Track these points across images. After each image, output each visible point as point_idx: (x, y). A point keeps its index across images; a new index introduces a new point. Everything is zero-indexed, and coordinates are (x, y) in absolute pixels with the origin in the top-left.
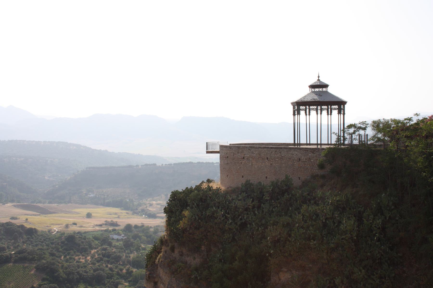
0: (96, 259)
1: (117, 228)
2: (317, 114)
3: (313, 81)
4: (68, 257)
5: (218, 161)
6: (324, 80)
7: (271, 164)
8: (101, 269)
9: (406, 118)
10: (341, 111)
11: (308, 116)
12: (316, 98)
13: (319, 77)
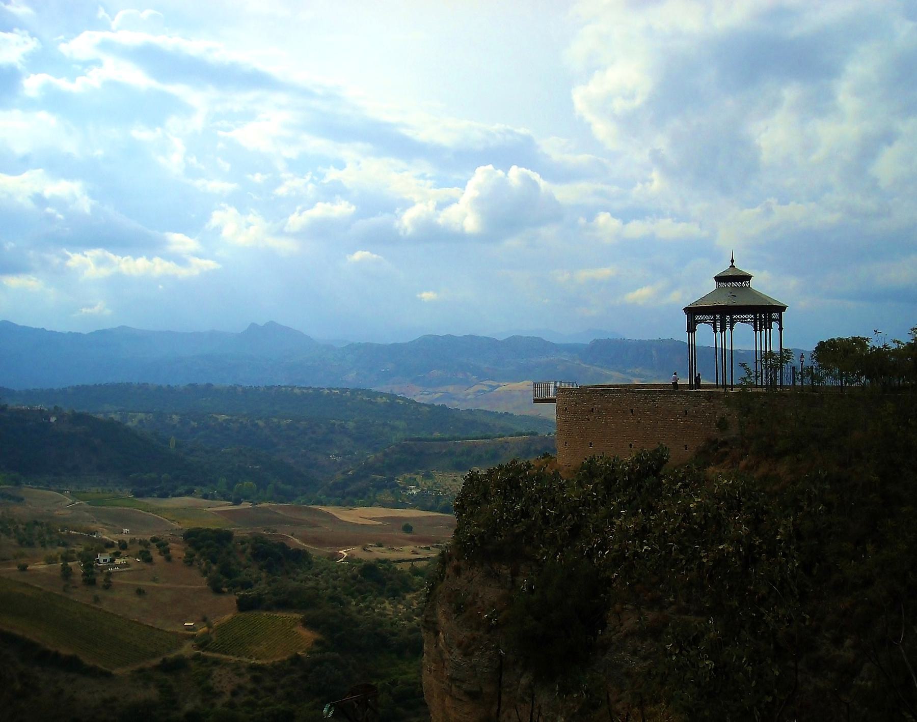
0: (413, 610)
3: (722, 268)
4: (362, 605)
5: (554, 417)
6: (743, 267)
7: (638, 422)
12: (724, 301)
13: (732, 261)
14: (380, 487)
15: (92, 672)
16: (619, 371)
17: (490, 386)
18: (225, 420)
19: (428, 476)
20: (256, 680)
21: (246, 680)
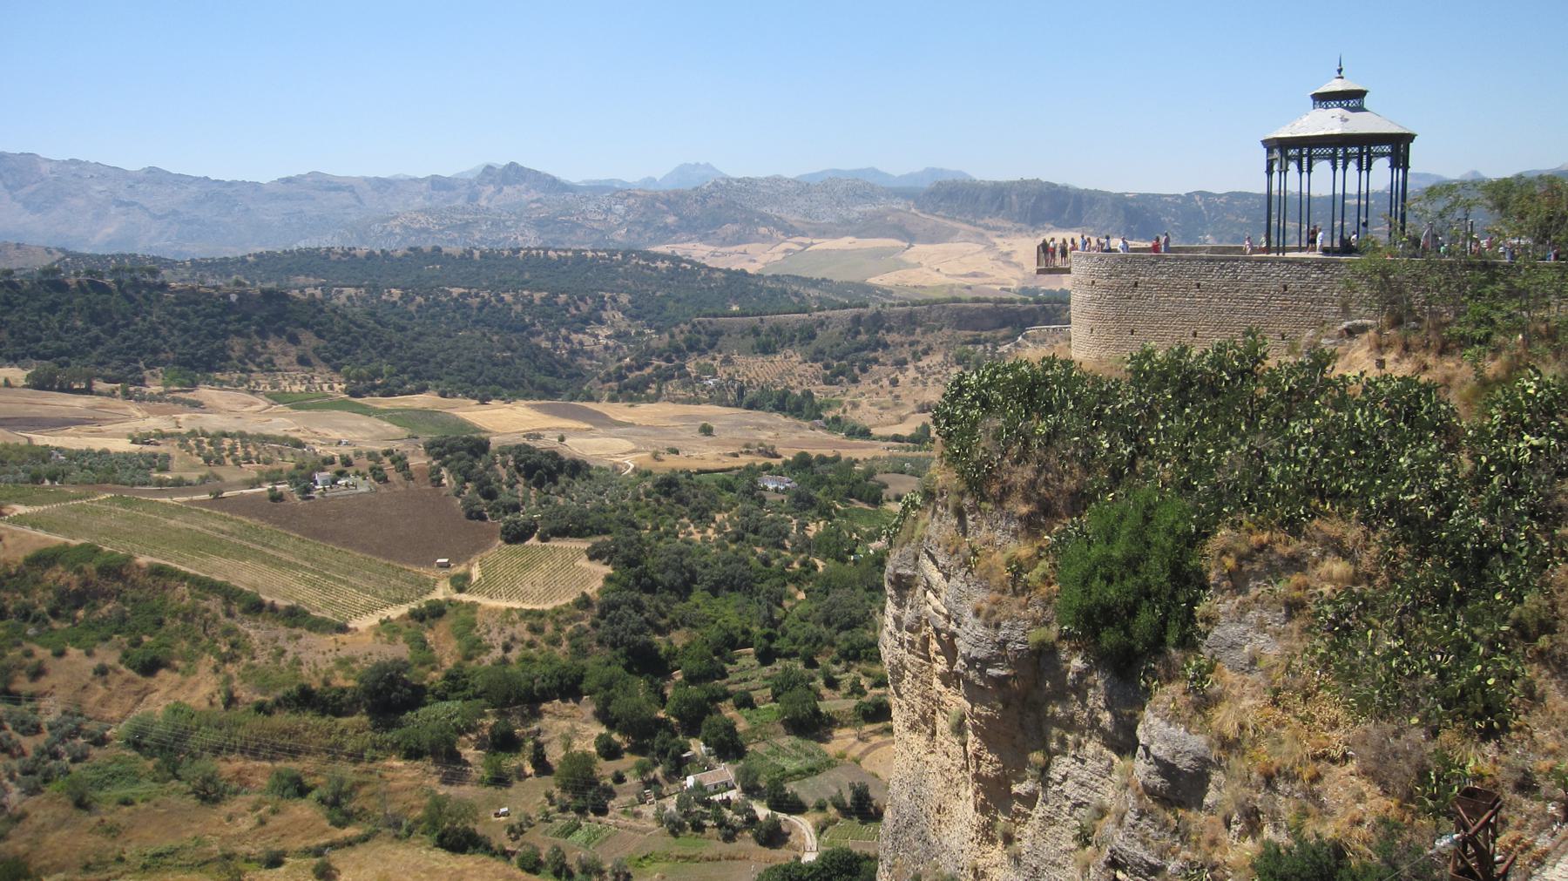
1: (774, 462)
2: (1335, 169)
8: (739, 561)
9: (1265, 168)
10: (1400, 160)
11: (1305, 175)
14: (665, 377)
15: (320, 626)
16: (968, 222)
17: (801, 244)
18: (461, 295)
19: (728, 361)
20: (534, 629)
21: (521, 630)
